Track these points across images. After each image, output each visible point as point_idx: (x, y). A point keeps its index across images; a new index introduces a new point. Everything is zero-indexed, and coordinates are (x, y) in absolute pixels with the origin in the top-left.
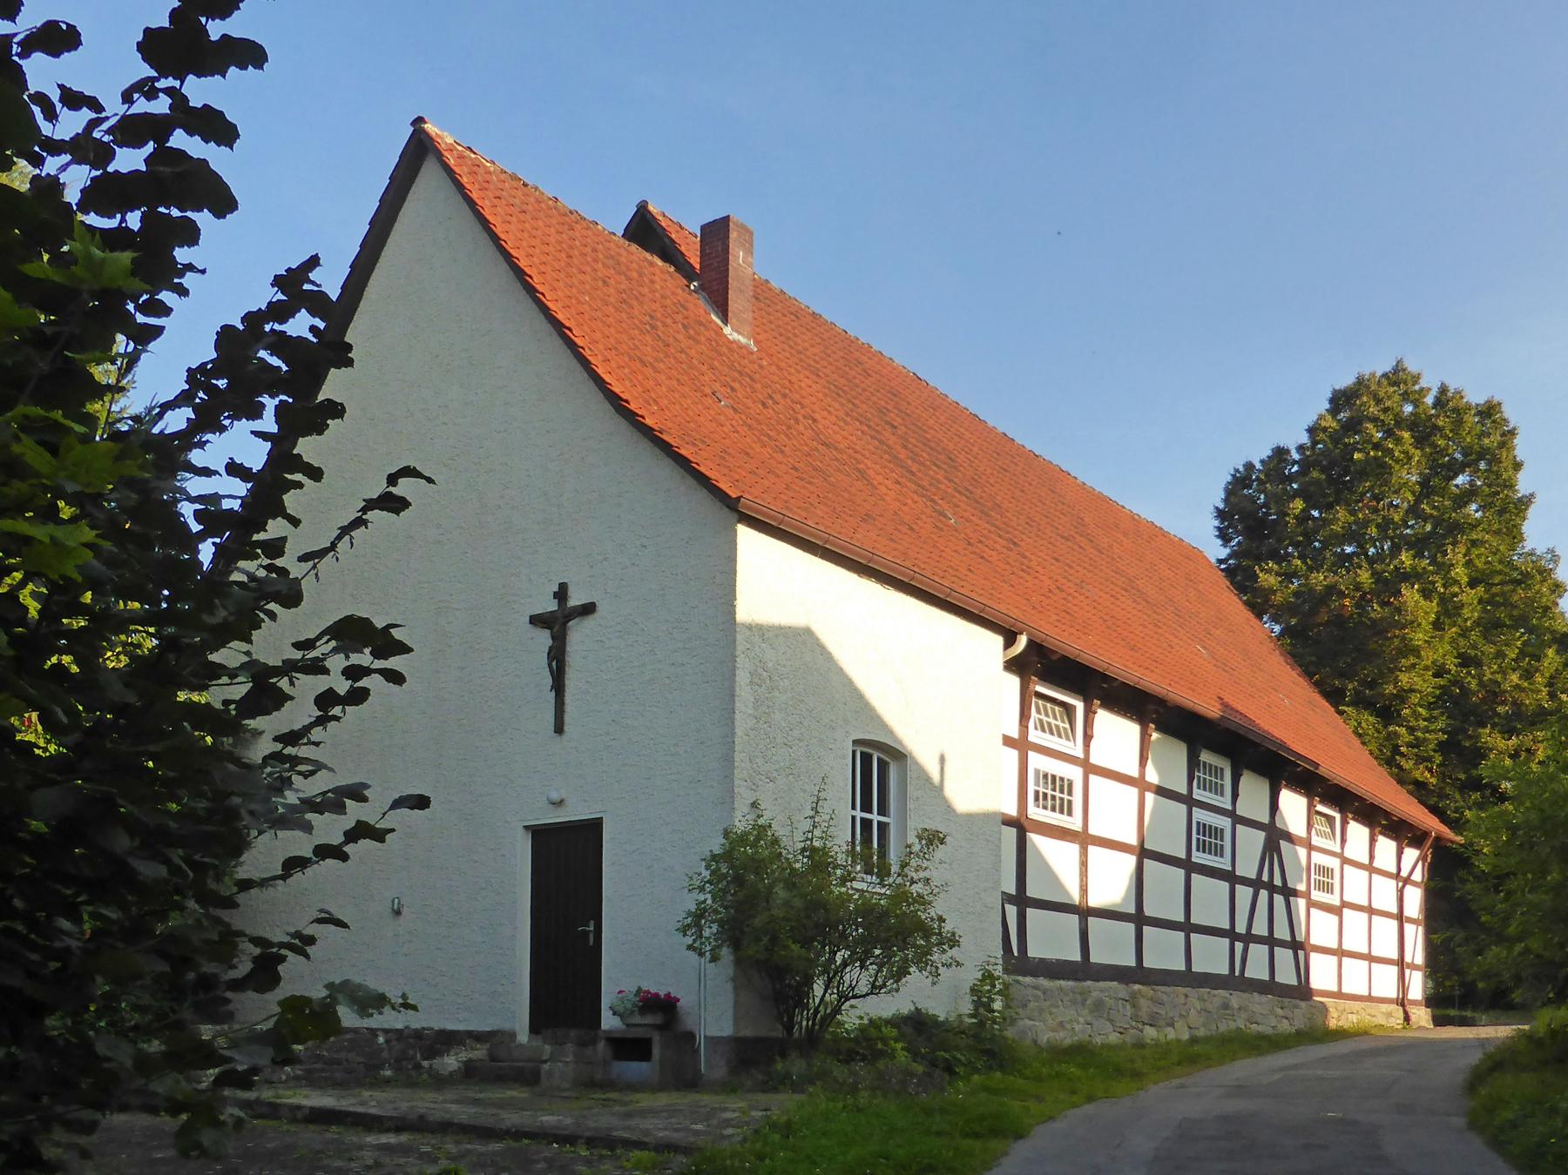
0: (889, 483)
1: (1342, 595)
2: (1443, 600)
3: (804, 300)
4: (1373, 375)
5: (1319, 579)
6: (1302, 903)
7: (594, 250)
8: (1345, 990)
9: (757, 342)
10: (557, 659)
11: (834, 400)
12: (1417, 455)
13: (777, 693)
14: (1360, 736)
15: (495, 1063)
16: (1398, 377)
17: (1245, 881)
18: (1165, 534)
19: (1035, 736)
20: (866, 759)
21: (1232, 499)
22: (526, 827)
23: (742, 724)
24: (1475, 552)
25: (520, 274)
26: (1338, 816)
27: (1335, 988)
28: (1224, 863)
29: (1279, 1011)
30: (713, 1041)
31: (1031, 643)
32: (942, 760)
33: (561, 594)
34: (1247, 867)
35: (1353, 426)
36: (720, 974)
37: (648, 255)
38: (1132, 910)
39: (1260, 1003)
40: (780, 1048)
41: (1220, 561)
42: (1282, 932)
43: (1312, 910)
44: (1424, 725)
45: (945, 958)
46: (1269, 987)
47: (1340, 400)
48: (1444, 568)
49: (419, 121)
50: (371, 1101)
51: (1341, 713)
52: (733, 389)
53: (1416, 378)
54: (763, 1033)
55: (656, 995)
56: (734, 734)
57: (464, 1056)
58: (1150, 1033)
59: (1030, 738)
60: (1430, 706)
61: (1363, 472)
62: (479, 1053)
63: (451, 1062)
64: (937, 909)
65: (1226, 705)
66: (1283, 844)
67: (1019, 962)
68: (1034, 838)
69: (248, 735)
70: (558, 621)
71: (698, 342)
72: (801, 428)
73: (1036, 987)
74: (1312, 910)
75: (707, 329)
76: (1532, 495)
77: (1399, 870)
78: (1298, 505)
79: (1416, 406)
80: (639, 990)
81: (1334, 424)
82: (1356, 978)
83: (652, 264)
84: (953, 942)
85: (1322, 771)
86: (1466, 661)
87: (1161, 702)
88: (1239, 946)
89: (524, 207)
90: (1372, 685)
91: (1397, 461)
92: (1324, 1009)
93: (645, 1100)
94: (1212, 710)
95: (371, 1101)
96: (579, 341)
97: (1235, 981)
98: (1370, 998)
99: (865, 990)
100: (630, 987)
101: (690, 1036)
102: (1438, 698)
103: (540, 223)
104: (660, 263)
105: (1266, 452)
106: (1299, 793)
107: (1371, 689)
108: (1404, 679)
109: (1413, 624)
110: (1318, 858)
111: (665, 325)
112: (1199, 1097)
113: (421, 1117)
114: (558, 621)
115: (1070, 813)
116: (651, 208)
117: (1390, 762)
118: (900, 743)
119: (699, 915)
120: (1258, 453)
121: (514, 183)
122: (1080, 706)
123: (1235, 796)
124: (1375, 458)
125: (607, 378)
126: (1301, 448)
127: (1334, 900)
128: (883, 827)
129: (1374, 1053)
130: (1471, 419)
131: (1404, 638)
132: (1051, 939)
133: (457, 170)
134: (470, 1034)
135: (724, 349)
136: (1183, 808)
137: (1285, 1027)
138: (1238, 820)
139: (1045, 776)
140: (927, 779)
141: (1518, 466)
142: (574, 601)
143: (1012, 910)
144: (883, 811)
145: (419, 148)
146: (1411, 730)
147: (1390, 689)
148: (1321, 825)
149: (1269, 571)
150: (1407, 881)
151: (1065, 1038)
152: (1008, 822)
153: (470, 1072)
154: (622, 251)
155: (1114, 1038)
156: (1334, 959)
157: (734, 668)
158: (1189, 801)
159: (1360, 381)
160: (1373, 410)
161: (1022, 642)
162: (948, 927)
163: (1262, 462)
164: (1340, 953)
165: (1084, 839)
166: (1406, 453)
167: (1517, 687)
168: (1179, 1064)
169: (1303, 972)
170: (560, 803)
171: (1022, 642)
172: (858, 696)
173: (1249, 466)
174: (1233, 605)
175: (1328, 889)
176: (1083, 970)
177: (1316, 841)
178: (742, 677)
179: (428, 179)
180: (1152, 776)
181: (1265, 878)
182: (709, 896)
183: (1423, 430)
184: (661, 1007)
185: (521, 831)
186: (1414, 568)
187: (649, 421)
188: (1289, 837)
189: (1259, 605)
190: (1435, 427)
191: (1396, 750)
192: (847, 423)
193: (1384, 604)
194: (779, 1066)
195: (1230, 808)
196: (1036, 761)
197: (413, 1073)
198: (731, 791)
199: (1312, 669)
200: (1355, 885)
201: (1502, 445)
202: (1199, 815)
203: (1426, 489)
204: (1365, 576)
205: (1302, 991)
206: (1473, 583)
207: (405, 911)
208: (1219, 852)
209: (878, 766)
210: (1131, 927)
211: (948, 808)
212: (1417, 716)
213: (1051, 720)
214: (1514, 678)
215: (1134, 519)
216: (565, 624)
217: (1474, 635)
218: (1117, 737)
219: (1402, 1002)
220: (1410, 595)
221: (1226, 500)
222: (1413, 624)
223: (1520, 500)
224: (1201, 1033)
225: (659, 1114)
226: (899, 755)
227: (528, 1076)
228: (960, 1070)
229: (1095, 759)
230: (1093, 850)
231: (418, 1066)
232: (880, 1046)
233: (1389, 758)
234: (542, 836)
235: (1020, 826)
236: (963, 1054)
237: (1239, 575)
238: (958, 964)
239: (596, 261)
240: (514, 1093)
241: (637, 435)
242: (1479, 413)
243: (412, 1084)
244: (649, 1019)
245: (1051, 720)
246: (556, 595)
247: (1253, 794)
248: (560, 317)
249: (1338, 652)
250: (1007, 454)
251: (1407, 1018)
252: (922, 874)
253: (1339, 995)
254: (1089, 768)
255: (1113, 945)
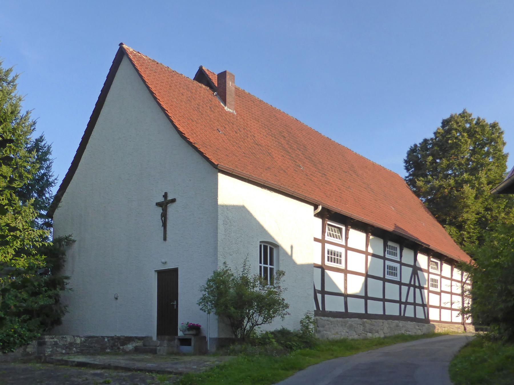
0: (279, 157)
1: (444, 188)
2: (478, 189)
3: (257, 96)
4: (456, 114)
5: (436, 183)
6: (426, 291)
7: (180, 84)
8: (442, 320)
9: (236, 111)
10: (164, 216)
11: (264, 129)
12: (469, 141)
13: (233, 227)
14: (451, 235)
15: (145, 347)
16: (464, 115)
17: (405, 285)
18: (384, 169)
19: (327, 238)
20: (265, 248)
21: (410, 157)
22: (156, 271)
23: (220, 237)
24: (489, 173)
25: (152, 93)
26: (439, 262)
27: (438, 319)
28: (397, 279)
29: (418, 327)
30: (210, 339)
31: (323, 208)
32: (292, 247)
33: (165, 196)
34: (406, 279)
35: (449, 132)
36: (213, 317)
37: (200, 84)
38: (363, 295)
39: (410, 325)
40: (232, 341)
41: (406, 177)
42: (419, 301)
43: (430, 294)
44: (471, 230)
45: (284, 312)
46: (414, 319)
47: (445, 123)
48: (478, 179)
49: (121, 44)
50: (99, 360)
51: (444, 227)
52: (225, 128)
53: (470, 115)
54: (228, 336)
55: (194, 324)
56: (217, 240)
57: (134, 344)
58: (369, 335)
59: (326, 239)
60: (474, 225)
61: (451, 148)
62: (140, 344)
63: (130, 347)
64: (282, 296)
65: (396, 227)
66: (419, 272)
67: (321, 312)
68: (327, 272)
69: (71, 242)
70: (165, 204)
71: (214, 113)
72: (249, 139)
73: (328, 321)
74: (430, 294)
75: (218, 108)
76: (508, 154)
77: (462, 280)
78: (430, 158)
79: (470, 125)
80: (188, 323)
81: (442, 131)
82: (446, 316)
83: (201, 87)
84: (287, 306)
85: (431, 247)
86: (487, 209)
87: (372, 226)
88: (403, 306)
89: (156, 71)
90: (455, 218)
91: (462, 143)
92: (434, 327)
93: (187, 359)
94: (390, 228)
95: (99, 360)
96: (169, 114)
97: (401, 318)
98: (451, 323)
99: (261, 323)
100: (185, 322)
101: (205, 337)
102: (477, 222)
103: (162, 76)
104: (204, 86)
105: (421, 141)
106: (425, 255)
107: (455, 219)
108: (465, 216)
109: (467, 198)
110: (431, 276)
111: (203, 107)
112: (362, 358)
113: (109, 365)
114: (165, 204)
115: (340, 263)
116: (203, 68)
117: (461, 244)
118: (277, 242)
119: (204, 299)
120: (418, 141)
121: (153, 63)
122: (344, 228)
123: (401, 256)
124: (456, 142)
125: (178, 126)
126: (432, 139)
127: (438, 290)
128: (271, 269)
129: (452, 340)
130: (487, 129)
131: (464, 202)
132: (333, 305)
133: (133, 60)
134: (136, 338)
135: (224, 115)
136: (382, 261)
137: (419, 333)
138: (402, 264)
139: (331, 252)
140: (286, 253)
141: (504, 144)
142: (170, 198)
143: (319, 296)
144: (271, 264)
145: (121, 53)
146: (469, 233)
147: (460, 219)
148: (432, 265)
149: (419, 181)
150: (465, 283)
151: (338, 337)
152: (316, 266)
153: (137, 350)
154: (191, 84)
155: (356, 337)
156: (438, 310)
157: (217, 219)
158: (384, 258)
159: (452, 117)
160: (455, 126)
161: (320, 208)
162: (285, 302)
163: (420, 144)
164: (440, 308)
165: (346, 272)
166: (465, 140)
167: (504, 218)
168: (376, 345)
169: (426, 314)
170: (165, 263)
171: (320, 208)
172: (262, 227)
173: (416, 146)
174: (408, 193)
175: (436, 286)
176: (346, 315)
177: (431, 270)
178: (220, 222)
179: (124, 64)
180: (370, 250)
181: (412, 283)
182: (207, 293)
183: (471, 133)
184: (195, 329)
185: (153, 272)
186: (468, 178)
187: (191, 140)
188: (421, 269)
189: (418, 193)
190: (476, 132)
191: (463, 240)
192: (267, 137)
193: (457, 191)
194: (231, 347)
195: (399, 260)
196: (328, 246)
197: (117, 350)
198: (216, 259)
199: (435, 213)
200: (445, 285)
201: (498, 137)
202: (388, 263)
203: (473, 152)
204: (452, 182)
205: (427, 320)
206: (488, 184)
207: (119, 298)
208: (395, 275)
209: (269, 250)
210: (369, 295)
211: (294, 263)
212: (470, 228)
213: (334, 233)
214: (503, 215)
215: (374, 164)
216: (166, 206)
217: (490, 201)
218: (357, 238)
219: (463, 324)
220: (466, 188)
221: (408, 157)
222: (467, 198)
223: (503, 155)
224: (388, 335)
225: (190, 363)
226: (277, 246)
227: (154, 351)
228: (294, 348)
229: (349, 245)
230: (349, 275)
231: (119, 348)
232: (267, 340)
233: (461, 243)
234: (160, 273)
235: (322, 268)
236: (298, 344)
237: (411, 182)
238: (289, 314)
239: (180, 87)
240: (147, 357)
241: (187, 145)
242: (491, 126)
243: (116, 354)
244: (191, 332)
245: (334, 233)
246: (164, 196)
247: (407, 256)
248: (164, 107)
249: (443, 208)
250: (328, 144)
251: (465, 329)
252: (278, 285)
253: (440, 321)
254: (347, 248)
255: (356, 307)
